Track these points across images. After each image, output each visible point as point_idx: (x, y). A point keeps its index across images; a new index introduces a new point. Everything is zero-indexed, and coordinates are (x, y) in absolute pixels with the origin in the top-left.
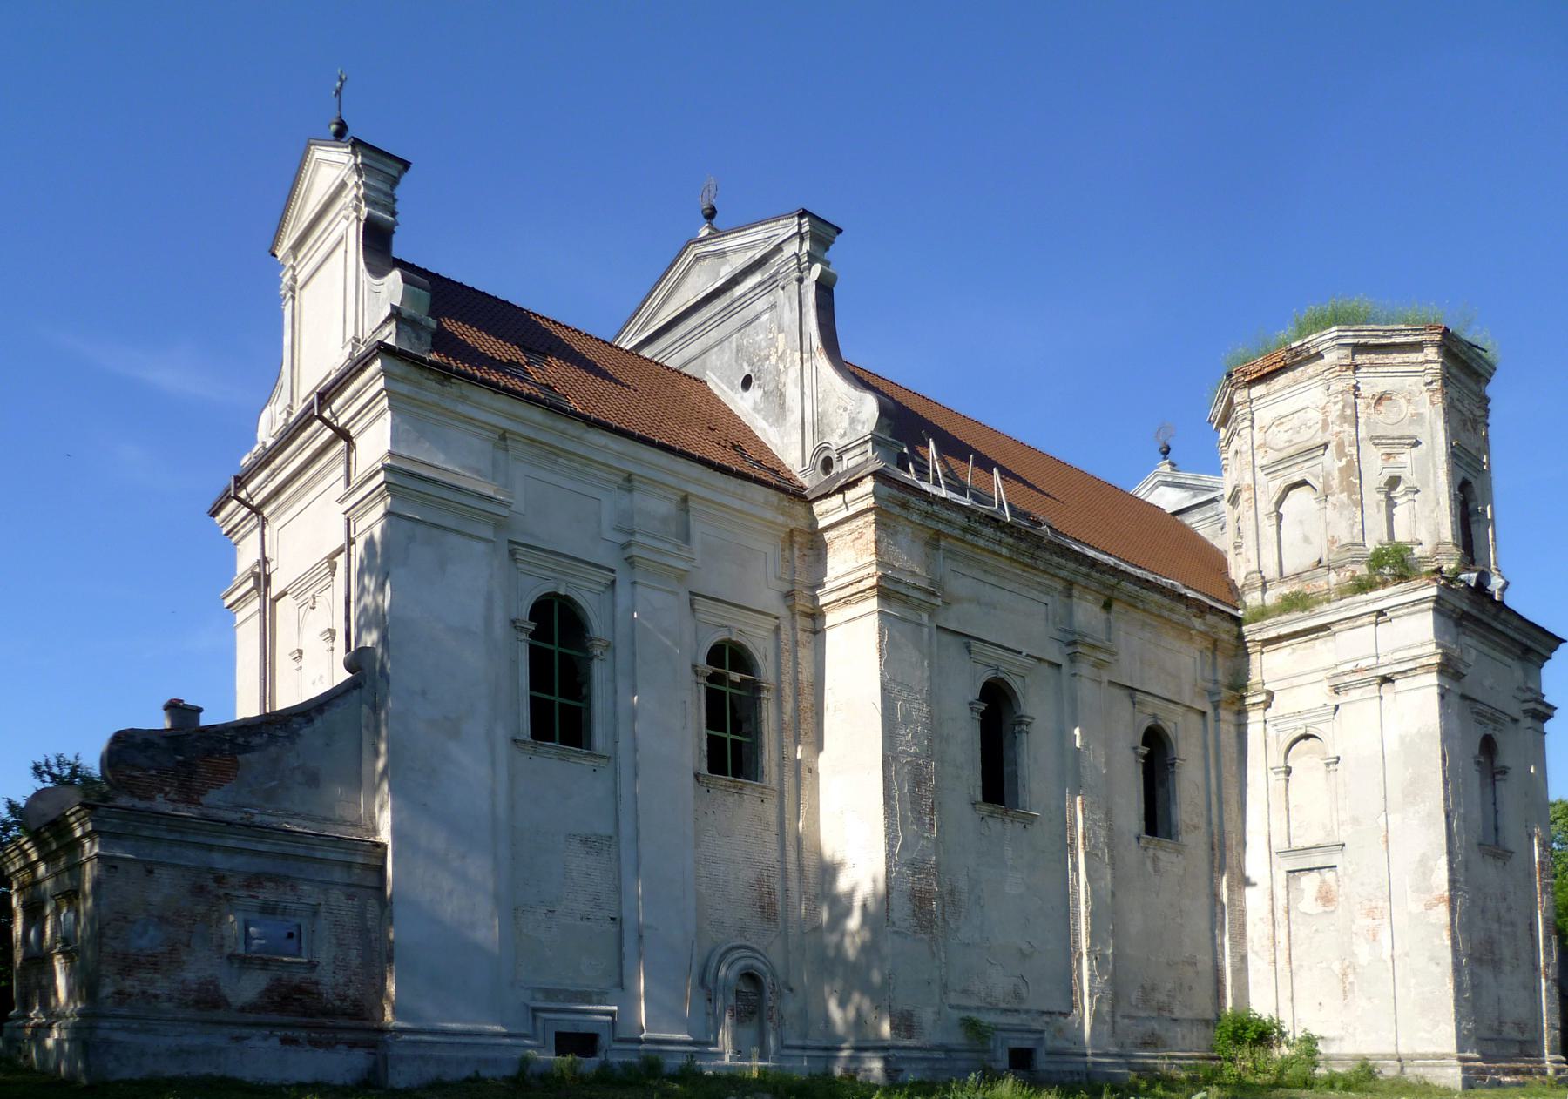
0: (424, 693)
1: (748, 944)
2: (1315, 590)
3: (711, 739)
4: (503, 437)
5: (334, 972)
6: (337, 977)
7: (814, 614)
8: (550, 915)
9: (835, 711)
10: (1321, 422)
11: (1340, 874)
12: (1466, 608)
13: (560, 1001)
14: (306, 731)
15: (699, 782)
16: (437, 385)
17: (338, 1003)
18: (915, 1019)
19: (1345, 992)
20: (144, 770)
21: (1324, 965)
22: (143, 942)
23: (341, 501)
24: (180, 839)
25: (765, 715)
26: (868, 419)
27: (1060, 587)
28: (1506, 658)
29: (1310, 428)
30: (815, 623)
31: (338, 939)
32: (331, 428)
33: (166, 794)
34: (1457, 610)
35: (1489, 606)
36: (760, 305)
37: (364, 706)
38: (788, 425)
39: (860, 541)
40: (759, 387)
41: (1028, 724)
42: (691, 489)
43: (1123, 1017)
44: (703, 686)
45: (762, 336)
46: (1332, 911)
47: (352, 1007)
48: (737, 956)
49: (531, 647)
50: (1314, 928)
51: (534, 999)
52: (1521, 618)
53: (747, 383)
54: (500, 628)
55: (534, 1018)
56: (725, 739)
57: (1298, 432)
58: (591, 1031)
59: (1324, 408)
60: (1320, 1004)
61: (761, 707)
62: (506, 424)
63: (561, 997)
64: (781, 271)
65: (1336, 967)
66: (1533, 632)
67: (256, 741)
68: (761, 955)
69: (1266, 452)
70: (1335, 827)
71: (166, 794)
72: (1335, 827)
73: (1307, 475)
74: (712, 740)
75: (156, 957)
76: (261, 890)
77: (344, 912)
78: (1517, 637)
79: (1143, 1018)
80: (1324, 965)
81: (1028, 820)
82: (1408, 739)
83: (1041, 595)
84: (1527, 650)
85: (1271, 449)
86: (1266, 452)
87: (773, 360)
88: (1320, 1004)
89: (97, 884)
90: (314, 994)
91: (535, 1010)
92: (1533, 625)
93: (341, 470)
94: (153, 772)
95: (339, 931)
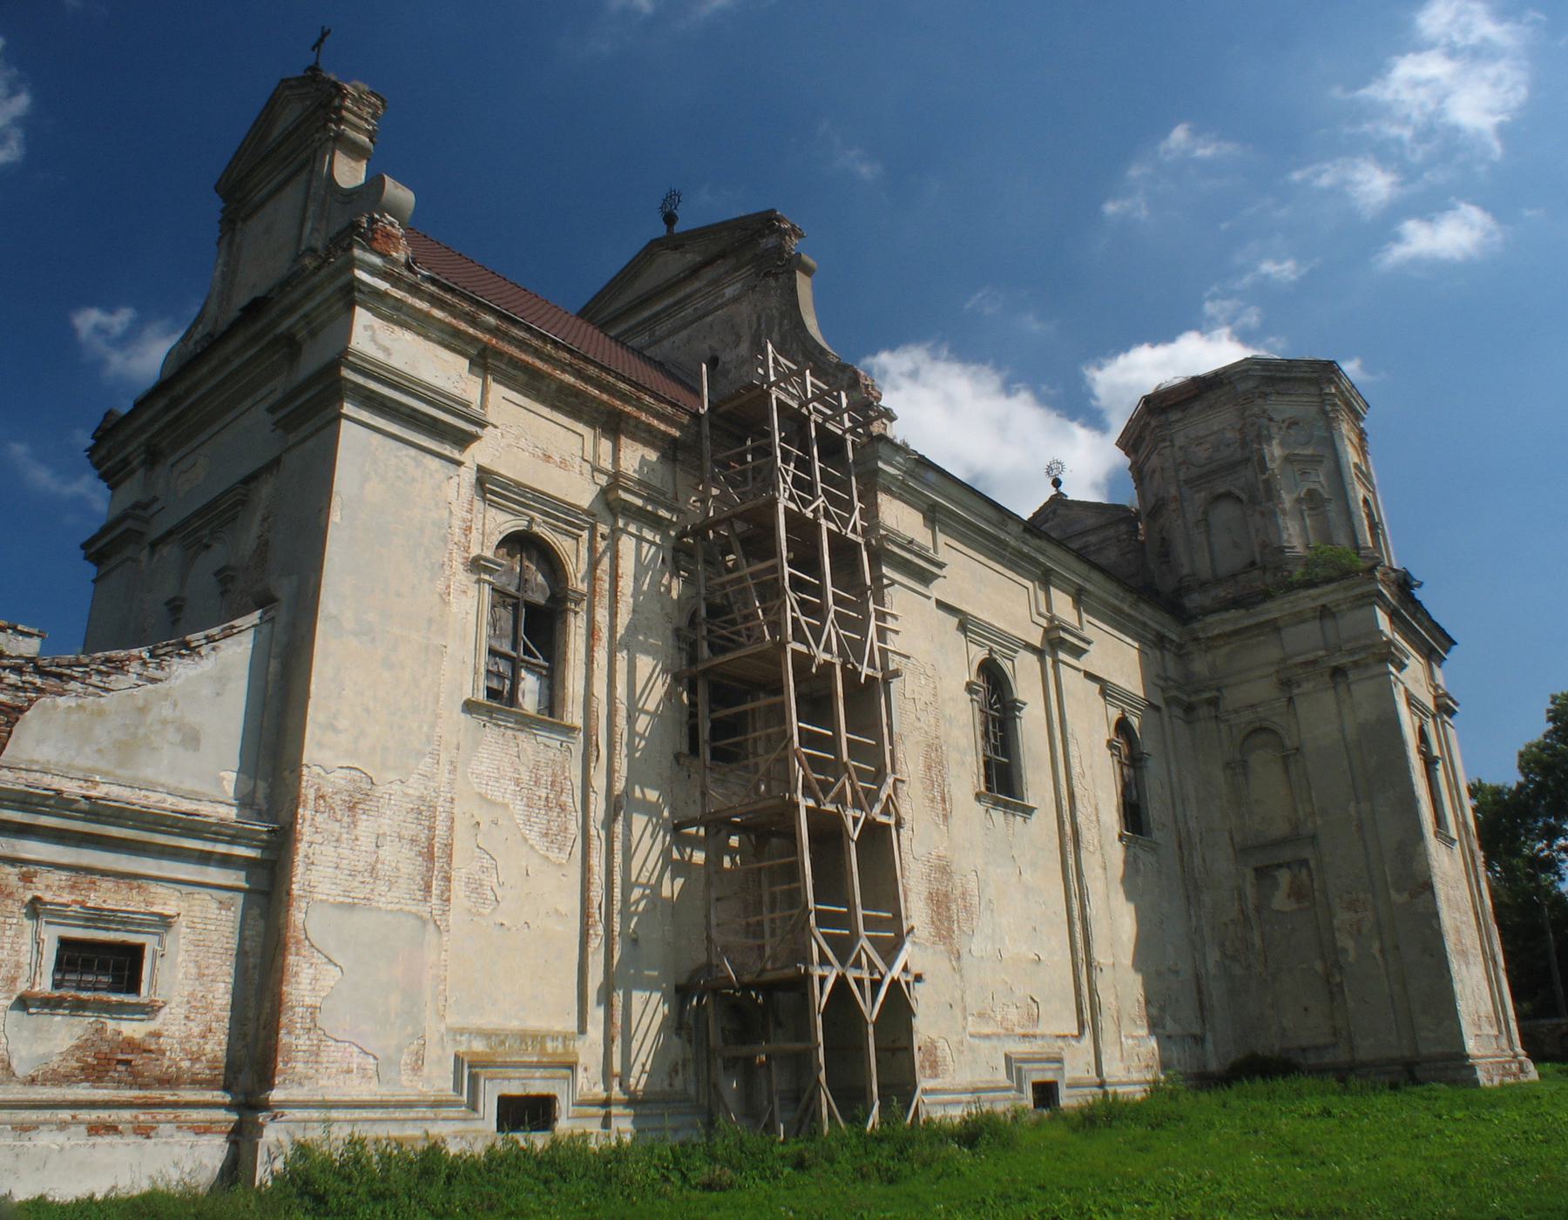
5: (187, 1018)
6: (191, 1024)
15: (678, 763)
27: (55, 1127)
31: (199, 967)
41: (1020, 709)
47: (208, 1072)
59: (1241, 429)
77: (213, 928)
80: (1305, 966)
88: (1306, 1009)
89: (525, 1154)
90: (150, 1051)
95: (202, 954)
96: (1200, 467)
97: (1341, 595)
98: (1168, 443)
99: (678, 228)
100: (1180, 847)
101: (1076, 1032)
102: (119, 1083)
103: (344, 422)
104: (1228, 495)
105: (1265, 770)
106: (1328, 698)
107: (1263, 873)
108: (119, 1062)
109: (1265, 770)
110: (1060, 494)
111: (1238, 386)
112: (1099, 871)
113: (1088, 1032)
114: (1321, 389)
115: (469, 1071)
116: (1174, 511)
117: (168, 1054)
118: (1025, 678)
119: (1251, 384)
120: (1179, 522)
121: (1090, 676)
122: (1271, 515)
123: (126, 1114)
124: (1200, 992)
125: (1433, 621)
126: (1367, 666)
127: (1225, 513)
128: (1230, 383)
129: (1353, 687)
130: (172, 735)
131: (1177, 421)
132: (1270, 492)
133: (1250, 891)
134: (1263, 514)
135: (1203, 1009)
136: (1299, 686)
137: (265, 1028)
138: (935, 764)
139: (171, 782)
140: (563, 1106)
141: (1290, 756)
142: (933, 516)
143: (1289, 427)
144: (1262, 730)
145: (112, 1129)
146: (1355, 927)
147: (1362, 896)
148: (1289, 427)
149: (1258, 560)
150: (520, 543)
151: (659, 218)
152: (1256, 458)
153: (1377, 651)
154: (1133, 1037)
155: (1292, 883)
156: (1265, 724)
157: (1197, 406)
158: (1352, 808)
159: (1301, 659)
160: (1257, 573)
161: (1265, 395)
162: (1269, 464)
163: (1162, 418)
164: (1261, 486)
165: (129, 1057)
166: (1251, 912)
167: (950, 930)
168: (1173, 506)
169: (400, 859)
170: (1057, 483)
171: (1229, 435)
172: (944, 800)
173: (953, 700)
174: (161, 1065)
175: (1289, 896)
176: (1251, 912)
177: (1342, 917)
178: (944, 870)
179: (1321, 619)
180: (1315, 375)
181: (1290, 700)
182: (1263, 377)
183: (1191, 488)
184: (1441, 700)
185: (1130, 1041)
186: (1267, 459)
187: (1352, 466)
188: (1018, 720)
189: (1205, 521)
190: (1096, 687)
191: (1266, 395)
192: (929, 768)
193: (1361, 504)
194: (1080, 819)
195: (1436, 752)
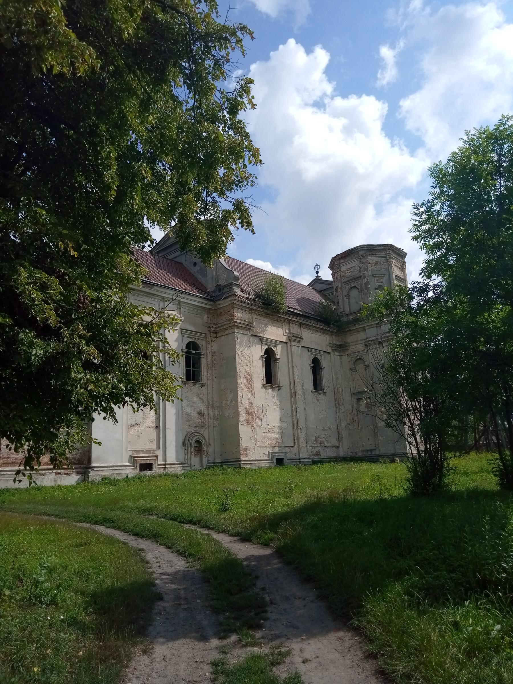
81: (279, 388)
91: (134, 457)
104: (355, 287)
110: (318, 276)
113: (296, 446)
115: (133, 459)
124: (338, 434)
135: (340, 438)
138: (249, 379)
140: (155, 466)
143: (375, 265)
148: (375, 265)
154: (312, 446)
156: (361, 357)
157: (348, 258)
161: (367, 255)
167: (252, 421)
169: (170, 559)
170: (317, 272)
178: (250, 405)
187: (394, 277)
189: (348, 295)
190: (306, 349)
195: (39, 472)
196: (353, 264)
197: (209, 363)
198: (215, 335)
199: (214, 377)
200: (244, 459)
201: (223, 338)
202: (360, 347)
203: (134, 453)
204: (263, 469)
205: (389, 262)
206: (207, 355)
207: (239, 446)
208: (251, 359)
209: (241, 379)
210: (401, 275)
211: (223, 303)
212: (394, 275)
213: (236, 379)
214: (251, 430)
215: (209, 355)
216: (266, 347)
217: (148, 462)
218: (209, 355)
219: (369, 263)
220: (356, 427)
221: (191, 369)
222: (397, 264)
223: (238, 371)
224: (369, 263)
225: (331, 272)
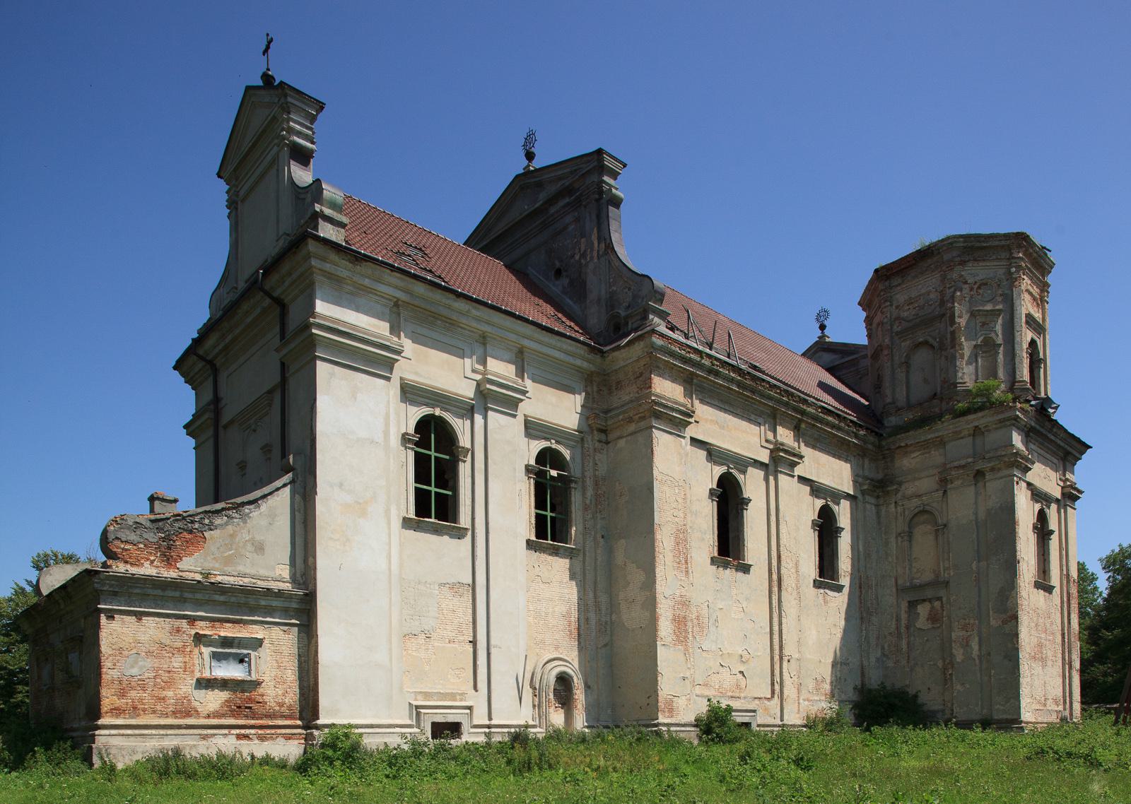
0: (341, 485)
1: (561, 656)
2: (932, 414)
3: (538, 516)
4: (396, 305)
7: (607, 430)
8: (428, 640)
9: (621, 496)
10: (939, 301)
11: (944, 602)
12: (1033, 424)
13: (434, 700)
14: (255, 514)
16: (351, 265)
17: (277, 708)
18: (674, 704)
19: (946, 680)
20: (135, 545)
21: (932, 663)
22: (135, 671)
23: (277, 350)
24: (161, 594)
25: (573, 499)
26: (646, 296)
28: (1053, 458)
29: (931, 305)
30: (607, 436)
32: (270, 298)
33: (152, 562)
34: (1028, 426)
35: (1047, 423)
36: (568, 219)
37: (297, 496)
38: (588, 301)
39: (641, 379)
40: (567, 276)
41: (747, 505)
42: (526, 343)
43: (804, 700)
44: (532, 479)
45: (568, 241)
46: (938, 627)
47: (287, 711)
48: (554, 665)
49: (416, 453)
50: (926, 639)
51: (416, 700)
52: (1066, 431)
53: (558, 273)
54: (395, 441)
55: (418, 714)
56: (430, 491)
57: (923, 309)
58: (456, 721)
60: (929, 689)
61: (570, 494)
62: (399, 294)
63: (435, 698)
64: (584, 194)
65: (940, 664)
66: (1074, 443)
67: (218, 521)
68: (570, 663)
69: (900, 322)
70: (942, 571)
71: (152, 562)
72: (942, 571)
73: (928, 337)
74: (538, 516)
75: (144, 681)
76: (223, 630)
78: (1062, 444)
79: (817, 700)
80: (932, 663)
81: (746, 569)
82: (993, 512)
83: (757, 417)
84: (1067, 453)
85: (904, 320)
86: (900, 322)
87: (577, 257)
88: (929, 689)
91: (417, 707)
92: (1073, 436)
93: (277, 329)
94: (142, 546)
96: (908, 321)
97: (990, 419)
98: (889, 303)
99: (537, 164)
100: (860, 588)
101: (769, 696)
102: (247, 717)
103: (319, 363)
104: (926, 343)
105: (924, 540)
106: (970, 492)
107: (912, 605)
108: (246, 708)
109: (924, 540)
111: (944, 257)
112: (794, 602)
114: (1011, 254)
116: (886, 355)
117: (268, 703)
118: (753, 485)
119: (955, 253)
120: (889, 364)
121: (802, 480)
122: (952, 360)
123: (253, 731)
125: (1069, 433)
126: (999, 469)
127: (922, 357)
128: (939, 253)
129: (987, 484)
130: (249, 547)
131: (897, 286)
132: (954, 343)
133: (904, 616)
134: (947, 358)
136: (952, 483)
137: (313, 690)
138: (681, 540)
139: (253, 572)
140: (465, 728)
141: (941, 529)
142: (691, 383)
143: (979, 288)
144: (924, 512)
145: (246, 737)
146: (965, 641)
147: (972, 621)
148: (979, 288)
149: (939, 392)
150: (424, 425)
151: (523, 154)
152: (948, 315)
153: (1007, 460)
154: (808, 700)
155: (931, 611)
156: (927, 508)
158: (974, 566)
159: (956, 464)
160: (935, 402)
161: (963, 263)
162: (957, 320)
163: (887, 283)
164: (949, 336)
165: (251, 705)
166: (903, 630)
167: (686, 638)
168: (886, 352)
170: (822, 327)
171: (932, 296)
172: (686, 563)
173: (699, 501)
174: (266, 709)
175: (928, 620)
176: (903, 630)
177: (957, 634)
178: (685, 603)
179: (974, 436)
180: (1008, 242)
181: (945, 492)
182: (965, 248)
183: (899, 338)
184: (1067, 490)
185: (806, 703)
186: (956, 315)
187: (1024, 316)
188: (745, 511)
189: (907, 364)
191: (965, 262)
192: (678, 544)
193: (1025, 346)
194: (783, 571)
196: (925, 286)
197: (588, 502)
198: (603, 437)
199: (599, 536)
200: (666, 721)
201: (622, 443)
202: (926, 484)
203: (419, 697)
204: (212, 681)
205: (1012, 281)
206: (584, 482)
207: (656, 691)
208: (688, 496)
209: (664, 540)
210: (1038, 315)
211: (626, 355)
212: (1024, 312)
213: (653, 541)
214: (682, 658)
215: (589, 482)
216: (723, 469)
217: (451, 719)
218: (589, 482)
219: (966, 283)
220: (904, 662)
221: (549, 514)
222: (1029, 287)
223: (656, 521)
224: (966, 283)
225: (864, 314)
